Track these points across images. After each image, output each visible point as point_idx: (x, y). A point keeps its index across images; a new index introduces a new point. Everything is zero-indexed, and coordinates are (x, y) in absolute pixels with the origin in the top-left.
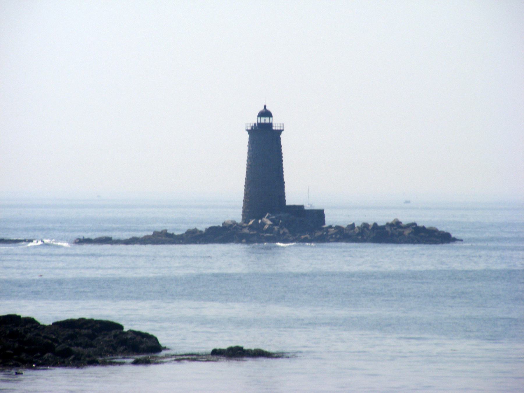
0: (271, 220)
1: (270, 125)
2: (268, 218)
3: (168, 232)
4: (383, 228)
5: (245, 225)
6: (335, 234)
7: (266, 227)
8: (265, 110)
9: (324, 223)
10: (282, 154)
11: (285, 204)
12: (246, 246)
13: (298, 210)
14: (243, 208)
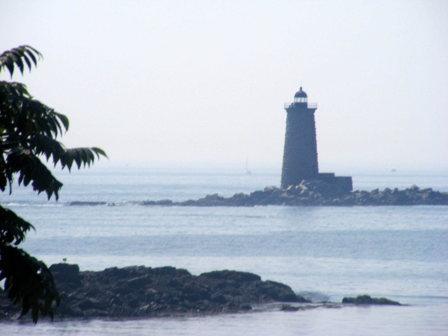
0: (307, 186)
1: (305, 104)
2: (304, 184)
3: (219, 195)
4: (403, 192)
5: (284, 190)
6: (361, 198)
7: (302, 192)
8: (301, 92)
9: (351, 188)
11: (317, 170)
12: (286, 207)
13: (330, 177)
14: (282, 175)
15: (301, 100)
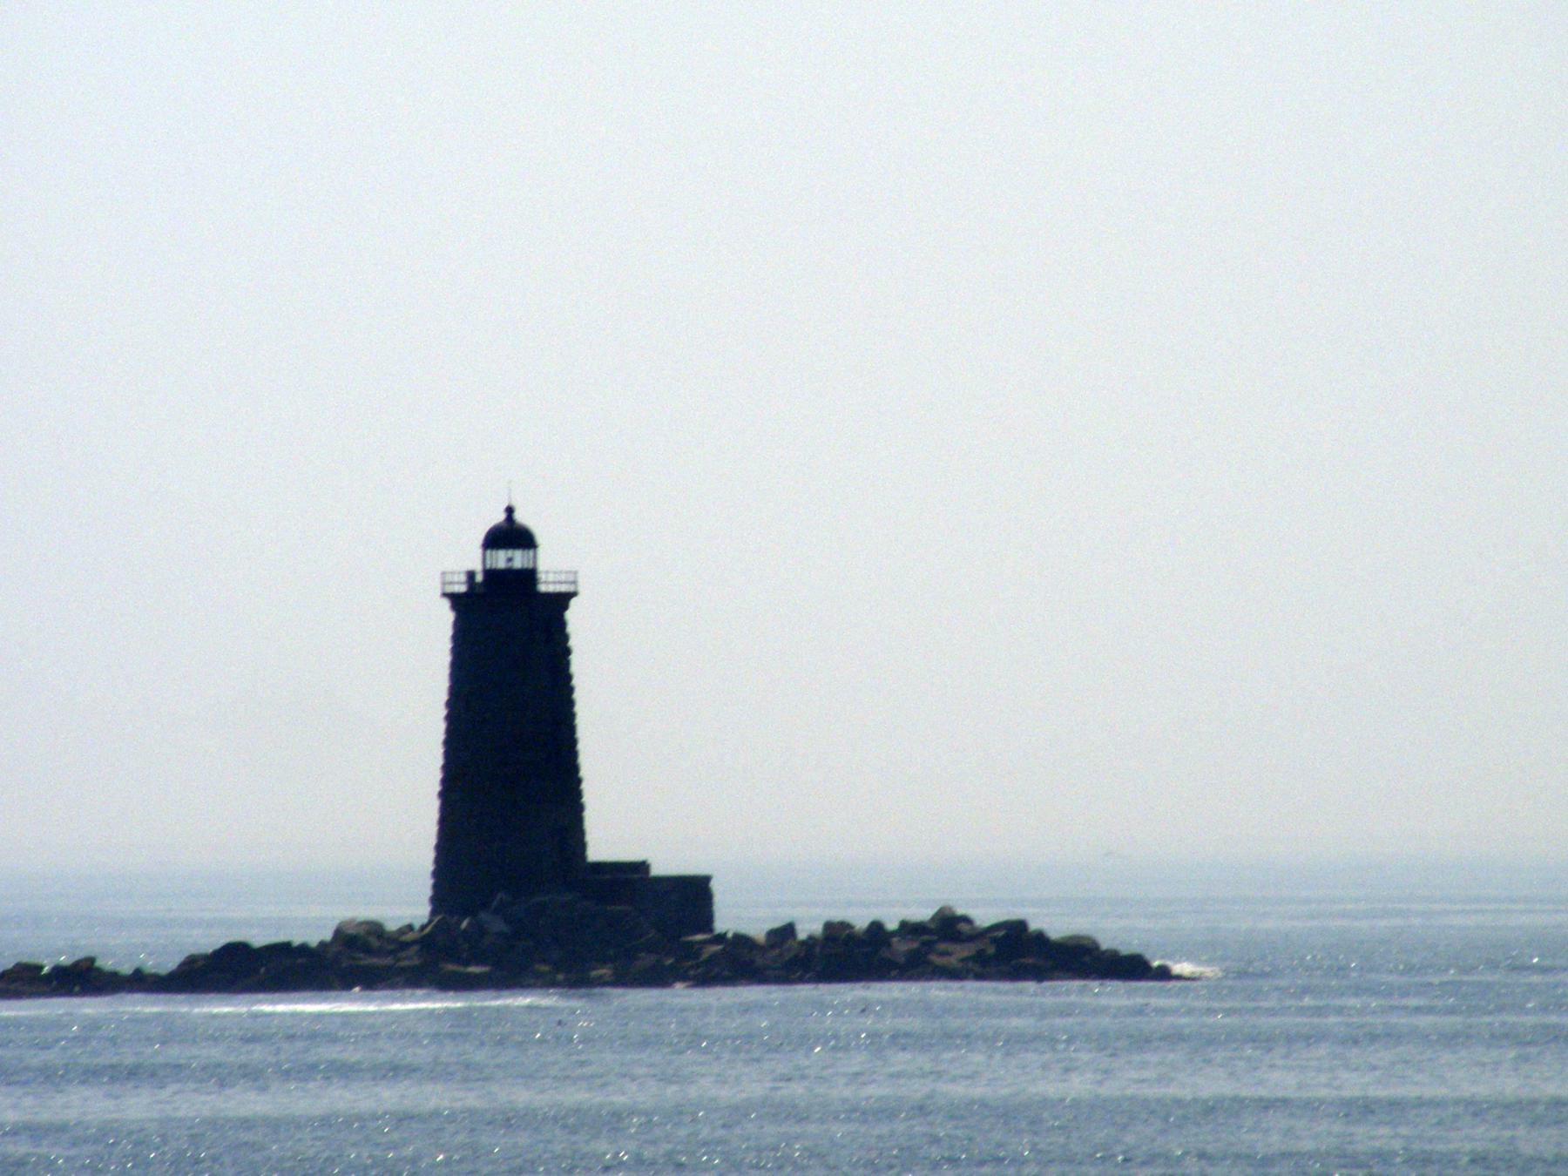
1: (529, 576)
10: (579, 781)
11: (582, 846)
15: (510, 560)
